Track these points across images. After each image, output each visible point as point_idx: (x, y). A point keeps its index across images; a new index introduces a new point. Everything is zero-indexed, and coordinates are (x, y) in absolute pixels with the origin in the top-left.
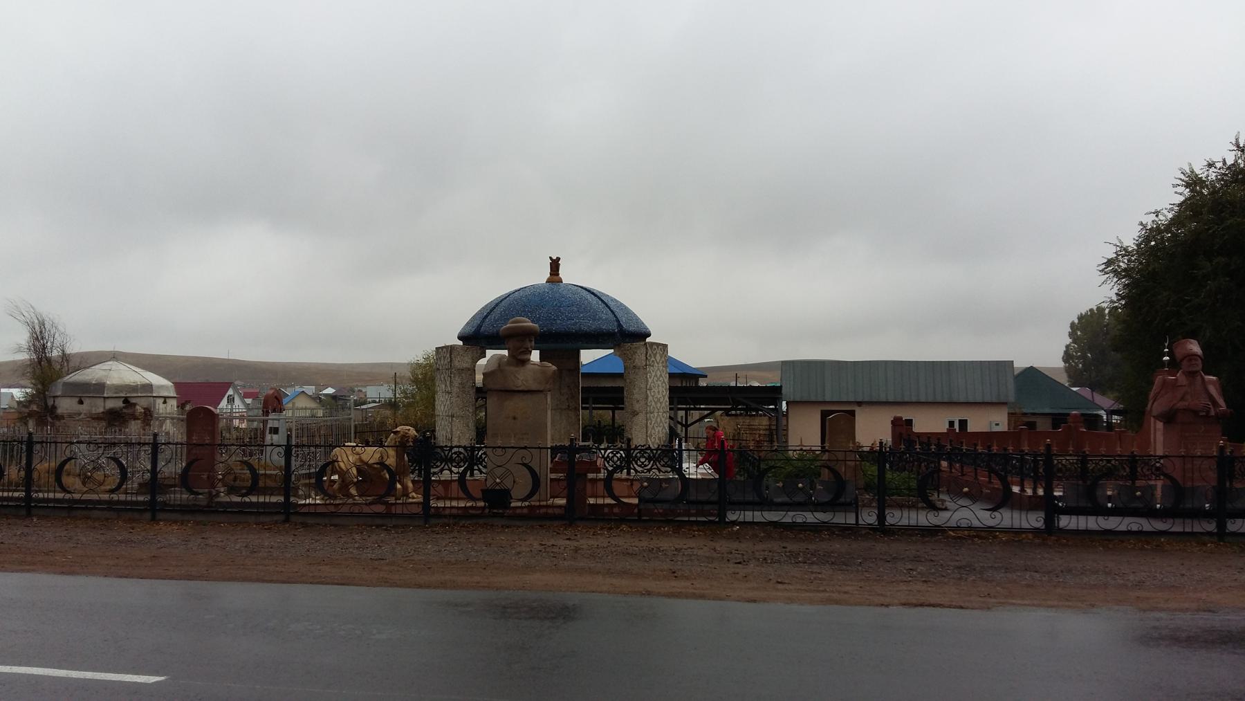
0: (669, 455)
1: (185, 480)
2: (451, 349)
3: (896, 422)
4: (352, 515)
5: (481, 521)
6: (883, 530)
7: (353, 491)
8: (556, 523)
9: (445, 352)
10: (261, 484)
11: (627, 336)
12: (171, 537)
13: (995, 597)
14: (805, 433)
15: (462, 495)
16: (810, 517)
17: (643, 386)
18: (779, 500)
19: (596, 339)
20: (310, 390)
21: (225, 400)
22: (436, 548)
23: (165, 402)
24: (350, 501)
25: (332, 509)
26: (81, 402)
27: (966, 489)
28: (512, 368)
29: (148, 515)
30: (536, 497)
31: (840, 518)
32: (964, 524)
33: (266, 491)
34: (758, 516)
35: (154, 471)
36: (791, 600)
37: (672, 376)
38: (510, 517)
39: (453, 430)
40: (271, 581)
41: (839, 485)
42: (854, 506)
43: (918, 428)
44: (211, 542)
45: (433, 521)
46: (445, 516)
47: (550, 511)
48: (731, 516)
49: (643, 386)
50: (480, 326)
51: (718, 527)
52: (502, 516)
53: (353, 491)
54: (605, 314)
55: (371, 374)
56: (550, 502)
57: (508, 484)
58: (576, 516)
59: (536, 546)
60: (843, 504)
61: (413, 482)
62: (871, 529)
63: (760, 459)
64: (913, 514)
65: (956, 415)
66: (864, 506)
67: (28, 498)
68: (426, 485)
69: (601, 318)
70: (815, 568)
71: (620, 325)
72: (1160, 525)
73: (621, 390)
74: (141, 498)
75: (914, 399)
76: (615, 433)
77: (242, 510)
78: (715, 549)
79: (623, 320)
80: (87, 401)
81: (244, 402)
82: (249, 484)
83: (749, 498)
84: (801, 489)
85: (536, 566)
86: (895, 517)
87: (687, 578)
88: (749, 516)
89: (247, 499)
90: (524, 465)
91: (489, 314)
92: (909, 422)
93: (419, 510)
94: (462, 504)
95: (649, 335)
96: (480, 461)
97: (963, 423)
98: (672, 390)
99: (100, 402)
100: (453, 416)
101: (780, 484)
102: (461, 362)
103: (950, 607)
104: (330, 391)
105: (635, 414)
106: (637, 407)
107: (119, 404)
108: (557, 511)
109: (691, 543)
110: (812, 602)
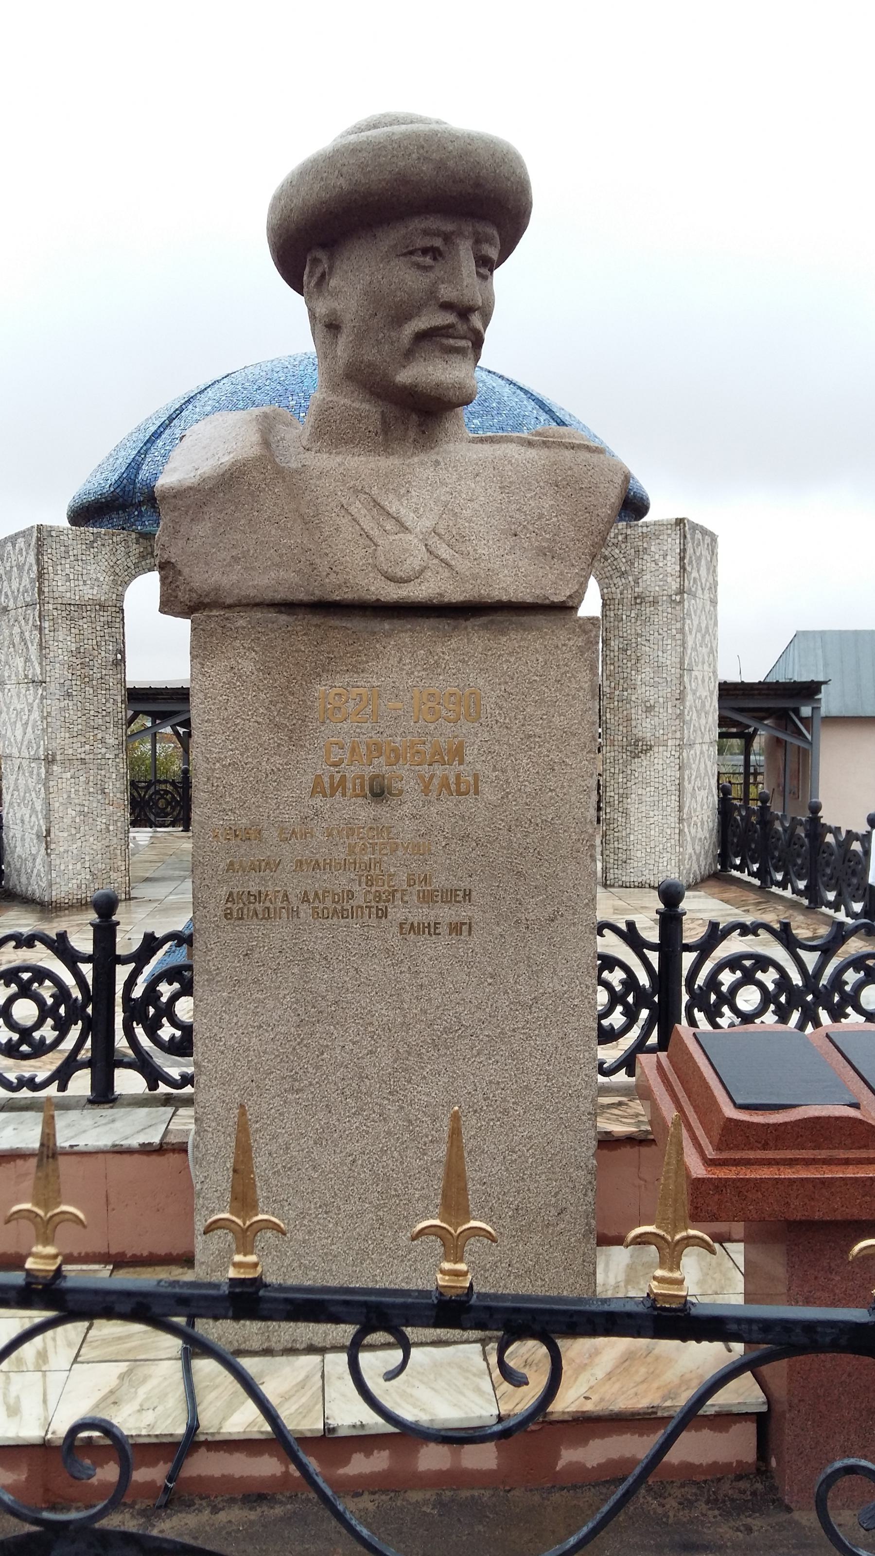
17: (670, 659)
49: (670, 659)
100: (50, 760)
105: (639, 748)
106: (645, 727)
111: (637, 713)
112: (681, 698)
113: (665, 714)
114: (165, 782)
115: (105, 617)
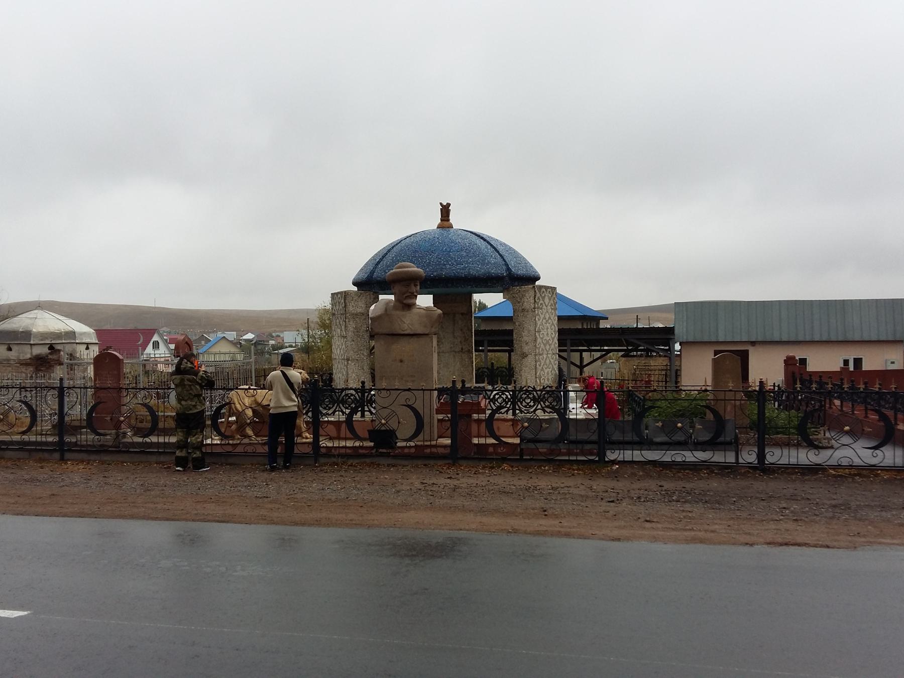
0: (555, 397)
1: (91, 423)
2: (345, 295)
3: (789, 362)
4: (246, 454)
5: (368, 460)
6: (762, 468)
7: (249, 432)
8: (440, 463)
9: (340, 298)
10: (161, 425)
11: (517, 280)
12: (75, 476)
13: (864, 536)
14: (697, 373)
15: (349, 435)
16: (689, 456)
17: (532, 328)
18: (658, 440)
19: (489, 283)
20: (232, 335)
21: (151, 344)
22: (321, 486)
23: (87, 348)
24: (246, 441)
25: (230, 449)
26: (10, 349)
27: (847, 428)
28: (398, 312)
29: (57, 455)
30: (420, 437)
31: (718, 457)
32: (845, 462)
33: (166, 432)
34: (637, 455)
35: (61, 414)
36: (655, 539)
37: (561, 319)
38: (395, 457)
39: (348, 375)
40: (156, 519)
41: (720, 423)
42: (735, 445)
43: (810, 368)
44: (111, 481)
45: (322, 460)
46: (334, 456)
47: (434, 450)
48: (611, 456)
49: (532, 328)
50: (372, 272)
51: (597, 465)
52: (388, 455)
53: (249, 432)
54: (494, 259)
55: (286, 320)
56: (434, 443)
57: (393, 425)
58: (461, 454)
59: (417, 484)
60: (721, 443)
61: (307, 423)
62: (752, 468)
63: (645, 400)
64: (793, 452)
65: (851, 354)
66: (743, 444)
67: (61, 442)
68: (316, 426)
69: (489, 262)
70: (687, 507)
71: (508, 269)
72: (702, 456)
73: (510, 332)
74: (50, 439)
75: (808, 338)
76: (507, 375)
77: (144, 451)
78: (591, 488)
79: (512, 264)
80: (14, 348)
81: (168, 348)
82: (149, 425)
83: (628, 438)
84: (680, 429)
85: (416, 504)
86: (774, 456)
87: (556, 516)
88: (628, 455)
89: (147, 440)
90: (409, 406)
91: (381, 260)
92: (803, 361)
93: (308, 450)
94: (349, 444)
95: (538, 278)
96: (371, 402)
97: (858, 362)
98: (561, 332)
99: (27, 349)
100: (348, 360)
101: (660, 424)
102: (356, 307)
103: (815, 546)
104: (250, 336)
105: (524, 356)
106: (526, 349)
107: (45, 350)
108: (441, 450)
109: (570, 482)
110: (676, 541)
111: (524, 345)
112: (535, 340)
113: (531, 345)
114: (351, 389)
115: (363, 317)
